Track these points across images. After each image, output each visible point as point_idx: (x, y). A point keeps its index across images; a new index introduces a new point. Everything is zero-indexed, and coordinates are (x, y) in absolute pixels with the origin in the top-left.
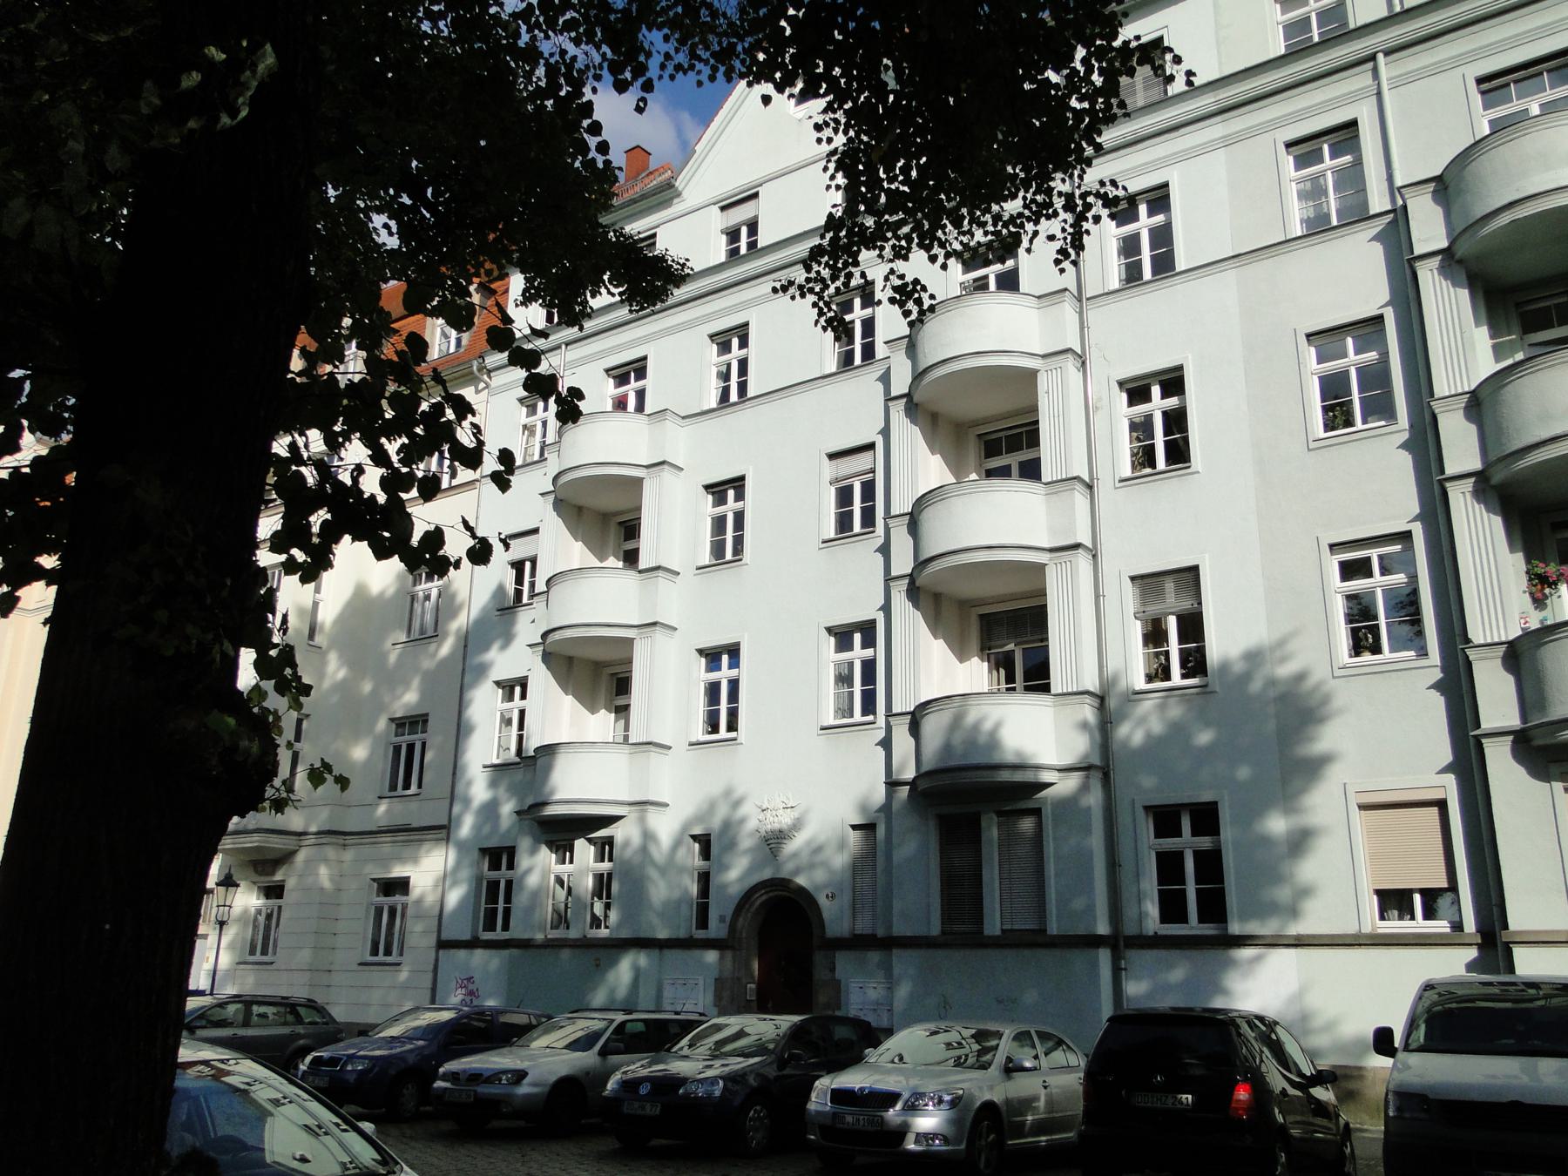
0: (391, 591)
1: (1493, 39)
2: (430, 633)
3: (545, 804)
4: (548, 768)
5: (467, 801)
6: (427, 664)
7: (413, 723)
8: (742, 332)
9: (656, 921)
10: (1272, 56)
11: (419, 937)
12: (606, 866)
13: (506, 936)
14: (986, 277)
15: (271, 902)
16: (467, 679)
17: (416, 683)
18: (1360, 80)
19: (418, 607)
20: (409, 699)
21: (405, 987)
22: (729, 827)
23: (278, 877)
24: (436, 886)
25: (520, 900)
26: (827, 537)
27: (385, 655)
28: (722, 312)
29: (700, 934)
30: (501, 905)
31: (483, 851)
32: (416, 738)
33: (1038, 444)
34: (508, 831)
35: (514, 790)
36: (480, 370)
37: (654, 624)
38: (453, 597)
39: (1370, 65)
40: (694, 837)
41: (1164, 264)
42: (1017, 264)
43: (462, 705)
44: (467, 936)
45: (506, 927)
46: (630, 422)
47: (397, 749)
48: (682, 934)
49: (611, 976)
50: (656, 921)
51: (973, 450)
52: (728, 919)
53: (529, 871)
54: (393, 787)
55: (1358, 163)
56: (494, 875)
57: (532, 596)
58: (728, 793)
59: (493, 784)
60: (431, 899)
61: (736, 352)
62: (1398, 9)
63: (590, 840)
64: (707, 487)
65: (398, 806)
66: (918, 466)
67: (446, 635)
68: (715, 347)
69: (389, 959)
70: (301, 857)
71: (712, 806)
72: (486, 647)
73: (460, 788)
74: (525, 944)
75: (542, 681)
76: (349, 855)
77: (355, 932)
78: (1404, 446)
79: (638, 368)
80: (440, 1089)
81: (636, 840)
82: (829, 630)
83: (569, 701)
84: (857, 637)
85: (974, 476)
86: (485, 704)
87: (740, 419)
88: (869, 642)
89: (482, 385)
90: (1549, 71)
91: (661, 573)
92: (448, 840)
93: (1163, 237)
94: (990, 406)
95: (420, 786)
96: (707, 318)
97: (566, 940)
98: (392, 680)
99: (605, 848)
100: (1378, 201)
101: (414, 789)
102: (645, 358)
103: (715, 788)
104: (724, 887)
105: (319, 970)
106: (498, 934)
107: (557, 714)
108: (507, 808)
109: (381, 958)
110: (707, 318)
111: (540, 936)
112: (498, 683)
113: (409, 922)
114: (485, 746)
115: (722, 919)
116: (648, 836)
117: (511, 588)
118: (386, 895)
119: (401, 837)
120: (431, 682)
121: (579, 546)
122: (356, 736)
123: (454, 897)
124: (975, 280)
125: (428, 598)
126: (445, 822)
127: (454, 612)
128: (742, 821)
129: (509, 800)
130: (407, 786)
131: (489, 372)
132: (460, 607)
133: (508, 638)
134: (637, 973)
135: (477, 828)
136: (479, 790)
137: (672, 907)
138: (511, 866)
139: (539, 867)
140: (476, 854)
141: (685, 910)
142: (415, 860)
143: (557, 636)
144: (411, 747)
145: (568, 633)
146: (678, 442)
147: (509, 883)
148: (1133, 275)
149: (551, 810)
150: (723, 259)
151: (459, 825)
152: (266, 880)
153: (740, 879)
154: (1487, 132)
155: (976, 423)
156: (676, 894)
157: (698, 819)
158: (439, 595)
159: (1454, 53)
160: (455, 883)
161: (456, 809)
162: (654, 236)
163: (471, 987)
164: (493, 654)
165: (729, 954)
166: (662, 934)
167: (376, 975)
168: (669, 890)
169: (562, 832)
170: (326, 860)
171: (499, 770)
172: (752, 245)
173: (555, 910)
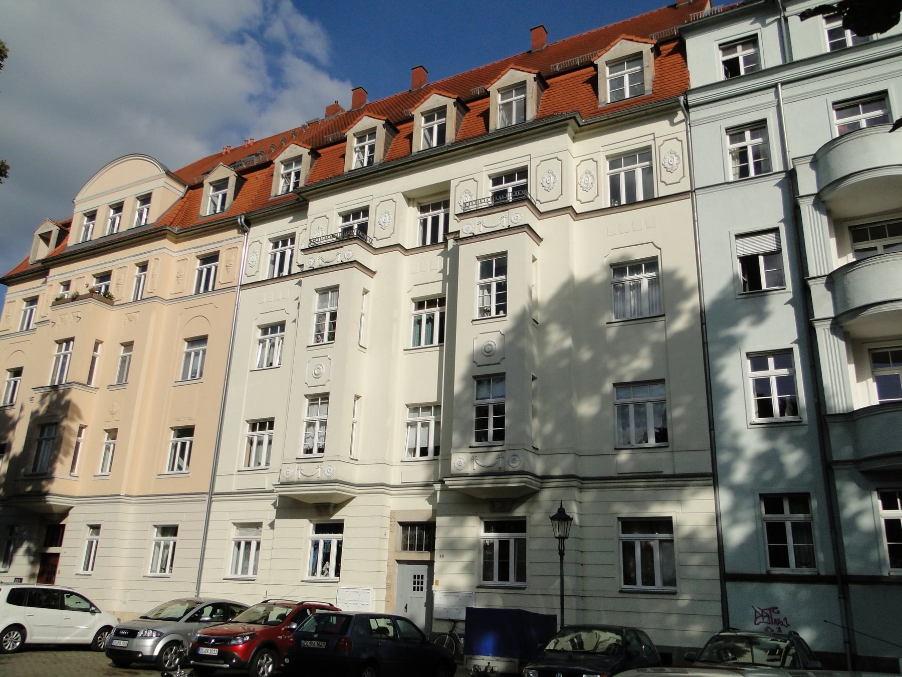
5: (737, 452)
14: (746, 147)
15: (504, 536)
16: (712, 349)
18: (770, 96)
20: (640, 364)
23: (519, 512)
27: (601, 332)
31: (763, 497)
39: (773, 89)
53: (859, 513)
55: (766, 142)
60: (708, 535)
62: (788, 61)
65: (644, 456)
67: (676, 314)
72: (734, 322)
73: (724, 439)
78: (790, 302)
90: (862, 104)
92: (715, 485)
96: (725, 116)
100: (777, 165)
106: (792, 569)
110: (725, 116)
120: (663, 351)
124: (741, 148)
129: (791, 451)
131: (687, 107)
135: (756, 475)
154: (838, 135)
155: (847, 220)
159: (801, 92)
160: (735, 522)
161: (723, 457)
164: (743, 328)
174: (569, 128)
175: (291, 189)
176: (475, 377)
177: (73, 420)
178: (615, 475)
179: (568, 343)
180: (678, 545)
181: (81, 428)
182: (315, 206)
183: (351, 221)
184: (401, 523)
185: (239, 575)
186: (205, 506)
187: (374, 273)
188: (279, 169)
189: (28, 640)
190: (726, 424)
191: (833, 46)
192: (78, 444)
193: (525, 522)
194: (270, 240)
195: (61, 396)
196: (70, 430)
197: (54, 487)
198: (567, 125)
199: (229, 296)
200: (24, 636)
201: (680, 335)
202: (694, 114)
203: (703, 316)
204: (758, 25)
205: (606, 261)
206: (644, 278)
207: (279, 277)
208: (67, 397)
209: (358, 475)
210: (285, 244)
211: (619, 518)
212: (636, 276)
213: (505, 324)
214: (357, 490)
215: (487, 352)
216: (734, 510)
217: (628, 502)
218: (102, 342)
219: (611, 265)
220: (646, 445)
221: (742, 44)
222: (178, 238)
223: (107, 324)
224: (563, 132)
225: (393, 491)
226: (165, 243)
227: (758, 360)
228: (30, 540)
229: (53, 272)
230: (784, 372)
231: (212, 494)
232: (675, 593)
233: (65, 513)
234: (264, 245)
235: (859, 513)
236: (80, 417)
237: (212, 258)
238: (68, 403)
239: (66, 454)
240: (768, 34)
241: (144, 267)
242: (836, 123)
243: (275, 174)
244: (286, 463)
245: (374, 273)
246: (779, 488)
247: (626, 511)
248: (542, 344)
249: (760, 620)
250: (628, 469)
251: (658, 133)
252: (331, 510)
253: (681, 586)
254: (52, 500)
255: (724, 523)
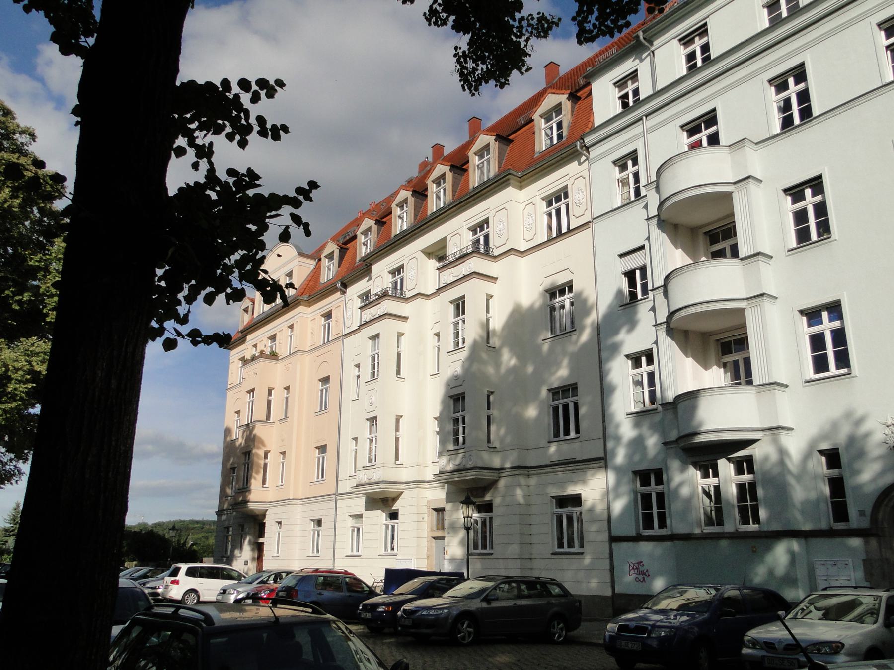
0: (538, 305)
1: (853, 16)
2: (569, 329)
3: (696, 434)
4: (693, 409)
5: (618, 439)
6: (572, 349)
7: (568, 389)
8: (799, 73)
9: (799, 516)
10: (760, 30)
11: (595, 534)
12: (747, 478)
13: (663, 532)
15: (483, 515)
17: (565, 362)
19: (557, 314)
20: (562, 374)
21: (589, 569)
22: (856, 444)
23: (488, 497)
24: (602, 499)
25: (674, 507)
26: (790, 247)
27: (539, 347)
28: (619, 146)
29: (841, 526)
30: (655, 510)
31: (635, 473)
32: (570, 401)
33: (735, 235)
34: (655, 457)
35: (654, 428)
36: (581, 148)
37: (762, 295)
38: (585, 301)
40: (821, 452)
41: (806, 113)
42: (807, 85)
43: (602, 374)
44: (633, 533)
45: (662, 524)
46: (708, 154)
47: (556, 410)
48: (824, 525)
49: (769, 559)
50: (799, 516)
51: (702, 241)
52: (868, 511)
53: (681, 484)
54: (557, 434)
56: (646, 489)
57: (645, 291)
58: (848, 415)
59: (637, 425)
60: (601, 507)
61: (631, 169)
63: (729, 460)
64: (786, 191)
65: (565, 447)
66: (666, 256)
67: (583, 328)
68: (617, 168)
69: (572, 550)
70: (502, 483)
71: (835, 426)
72: (616, 332)
73: (610, 430)
74: (687, 537)
75: (669, 352)
76: (533, 481)
77: (545, 535)
79: (711, 119)
80: (747, 655)
81: (774, 456)
82: (802, 312)
83: (690, 362)
84: (644, 359)
85: (704, 258)
86: (620, 372)
87: (806, 136)
88: (650, 361)
89: (583, 158)
91: (760, 257)
92: (606, 467)
93: (804, 96)
94: (706, 217)
95: (577, 432)
97: (723, 533)
98: (548, 363)
99: (745, 465)
101: (573, 434)
102: (714, 110)
103: (834, 411)
104: (859, 487)
105: (525, 558)
106: (656, 531)
107: (681, 372)
108: (652, 442)
109: (566, 549)
111: (697, 531)
112: (627, 356)
113: (585, 526)
114: (626, 400)
115: (862, 513)
116: (783, 452)
117: (626, 290)
118: (560, 508)
119: (571, 467)
120: (576, 360)
121: (679, 252)
122: (527, 403)
123: (618, 506)
125: (563, 307)
126: (602, 455)
127: (587, 311)
128: (867, 435)
129: (651, 436)
130: (567, 433)
131: (587, 149)
132: (591, 308)
133: (632, 324)
134: (793, 557)
135: (629, 457)
136: (627, 431)
137: (810, 507)
138: (659, 481)
139: (689, 482)
140: (631, 475)
141: (823, 506)
142: (584, 482)
143: (683, 313)
144: (566, 407)
145: (693, 310)
146: (755, 162)
147: (660, 496)
148: (787, 123)
149: (700, 439)
150: (767, 25)
151: (614, 454)
152: (478, 501)
153: (874, 480)
155: (701, 227)
156: (813, 495)
157: (824, 437)
158: (572, 304)
159: (675, 112)
160: (617, 496)
161: (610, 444)
162: (706, 24)
163: (641, 569)
164: (622, 336)
165: (874, 542)
166: (807, 527)
167: (564, 562)
168: (809, 490)
169: (706, 455)
170: (519, 485)
171: (640, 416)
172: (706, 59)
173: (705, 513)
174: (511, 181)
175: (555, 141)
176: (451, 397)
177: (259, 448)
178: (549, 463)
179: (513, 362)
180: (584, 517)
181: (266, 453)
182: (376, 268)
183: (479, 234)
184: (435, 509)
185: (355, 553)
186: (333, 504)
187: (496, 279)
188: (360, 239)
189: (201, 599)
190: (612, 416)
191: (771, 21)
192: (265, 465)
193: (580, 498)
194: (543, 199)
195: (251, 431)
196: (258, 455)
197: (252, 497)
198: (508, 179)
199: (338, 344)
200: (199, 597)
201: (585, 345)
202: (594, 152)
203: (598, 330)
204: (637, 61)
205: (542, 289)
206: (567, 299)
207: (560, 234)
208: (254, 432)
209: (404, 475)
210: (558, 199)
211: (553, 497)
212: (562, 298)
213: (463, 354)
214: (402, 486)
215: (456, 378)
216: (618, 484)
217: (554, 484)
218: (492, 297)
219: (546, 291)
220: (569, 437)
221: (631, 79)
222: (523, 182)
223: (273, 374)
224: (507, 186)
225: (427, 486)
226: (301, 309)
227: (636, 360)
228: (249, 534)
229: (249, 338)
230: (837, 324)
231: (337, 494)
232: (582, 554)
233: (264, 516)
234: (538, 205)
235: (681, 484)
236: (264, 445)
237: (561, 195)
238: (255, 436)
239: (257, 473)
240: (643, 68)
241: (291, 327)
242: (685, 141)
243: (536, 130)
244: (350, 472)
245: (496, 279)
246: (643, 467)
247: (555, 492)
248: (498, 365)
249: (632, 572)
250: (555, 458)
251: (567, 174)
252: (390, 502)
253: (587, 548)
254: (251, 506)
255: (611, 497)
